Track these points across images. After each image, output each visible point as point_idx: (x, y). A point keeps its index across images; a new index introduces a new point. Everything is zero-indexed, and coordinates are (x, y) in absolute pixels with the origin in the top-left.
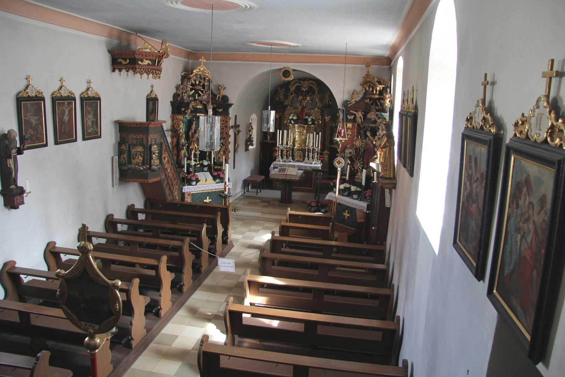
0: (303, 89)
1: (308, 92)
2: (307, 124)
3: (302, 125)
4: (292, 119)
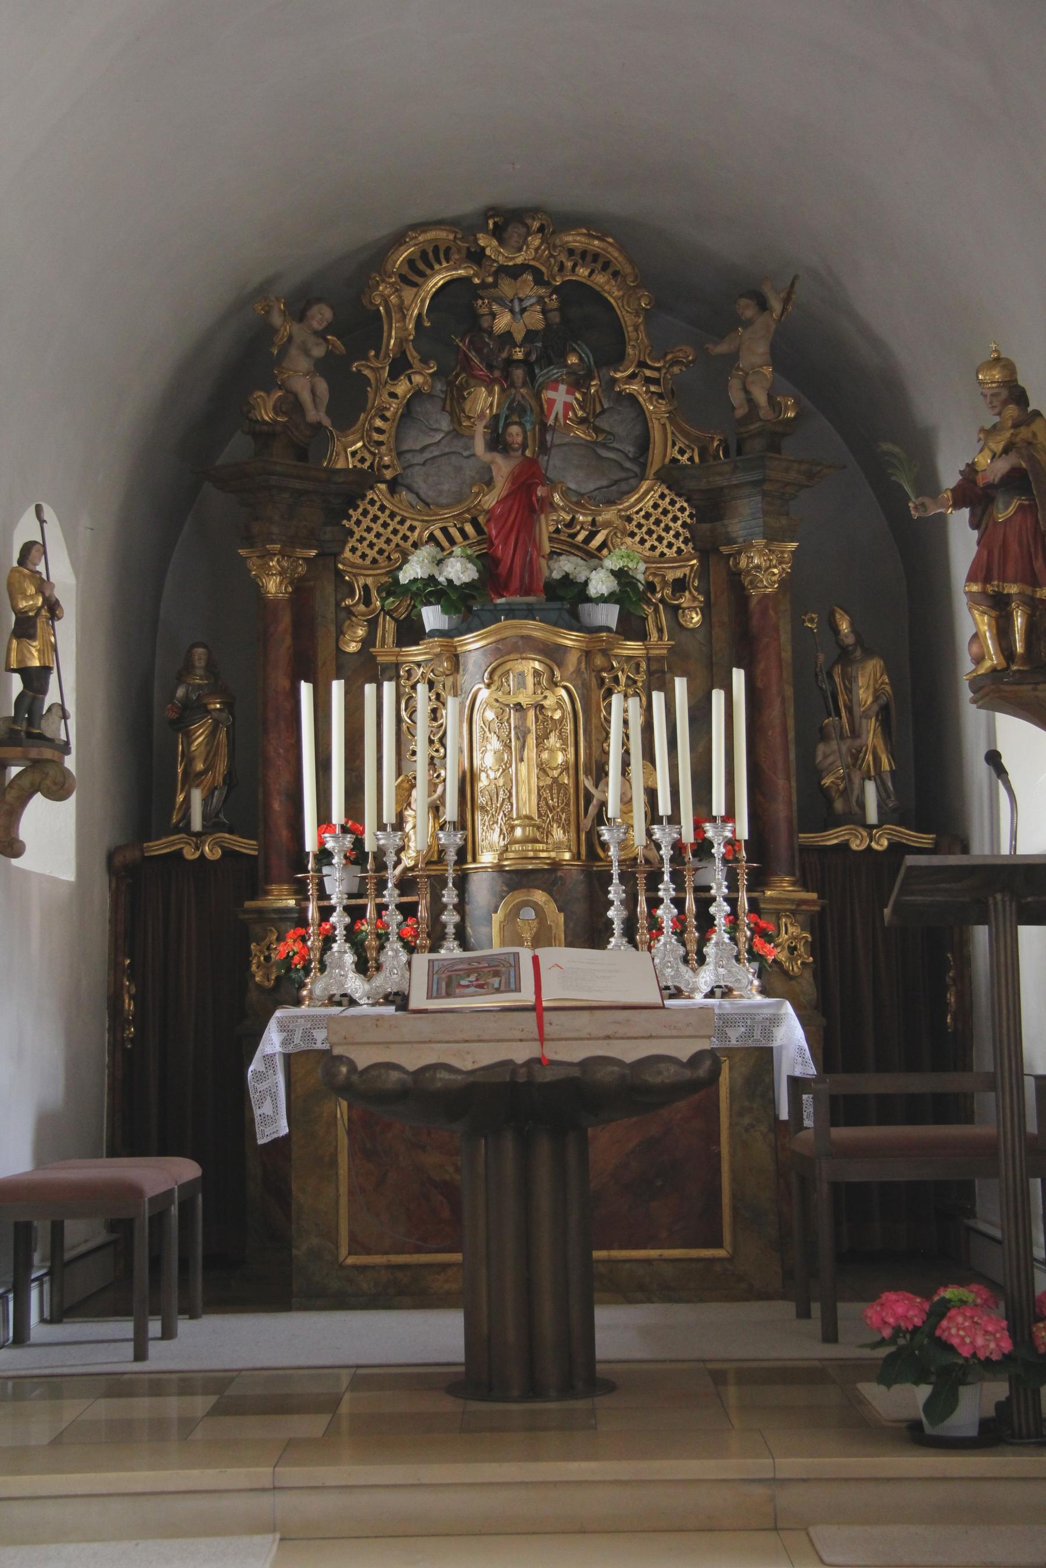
1: (549, 346)
2: (574, 622)
3: (534, 628)
4: (432, 590)
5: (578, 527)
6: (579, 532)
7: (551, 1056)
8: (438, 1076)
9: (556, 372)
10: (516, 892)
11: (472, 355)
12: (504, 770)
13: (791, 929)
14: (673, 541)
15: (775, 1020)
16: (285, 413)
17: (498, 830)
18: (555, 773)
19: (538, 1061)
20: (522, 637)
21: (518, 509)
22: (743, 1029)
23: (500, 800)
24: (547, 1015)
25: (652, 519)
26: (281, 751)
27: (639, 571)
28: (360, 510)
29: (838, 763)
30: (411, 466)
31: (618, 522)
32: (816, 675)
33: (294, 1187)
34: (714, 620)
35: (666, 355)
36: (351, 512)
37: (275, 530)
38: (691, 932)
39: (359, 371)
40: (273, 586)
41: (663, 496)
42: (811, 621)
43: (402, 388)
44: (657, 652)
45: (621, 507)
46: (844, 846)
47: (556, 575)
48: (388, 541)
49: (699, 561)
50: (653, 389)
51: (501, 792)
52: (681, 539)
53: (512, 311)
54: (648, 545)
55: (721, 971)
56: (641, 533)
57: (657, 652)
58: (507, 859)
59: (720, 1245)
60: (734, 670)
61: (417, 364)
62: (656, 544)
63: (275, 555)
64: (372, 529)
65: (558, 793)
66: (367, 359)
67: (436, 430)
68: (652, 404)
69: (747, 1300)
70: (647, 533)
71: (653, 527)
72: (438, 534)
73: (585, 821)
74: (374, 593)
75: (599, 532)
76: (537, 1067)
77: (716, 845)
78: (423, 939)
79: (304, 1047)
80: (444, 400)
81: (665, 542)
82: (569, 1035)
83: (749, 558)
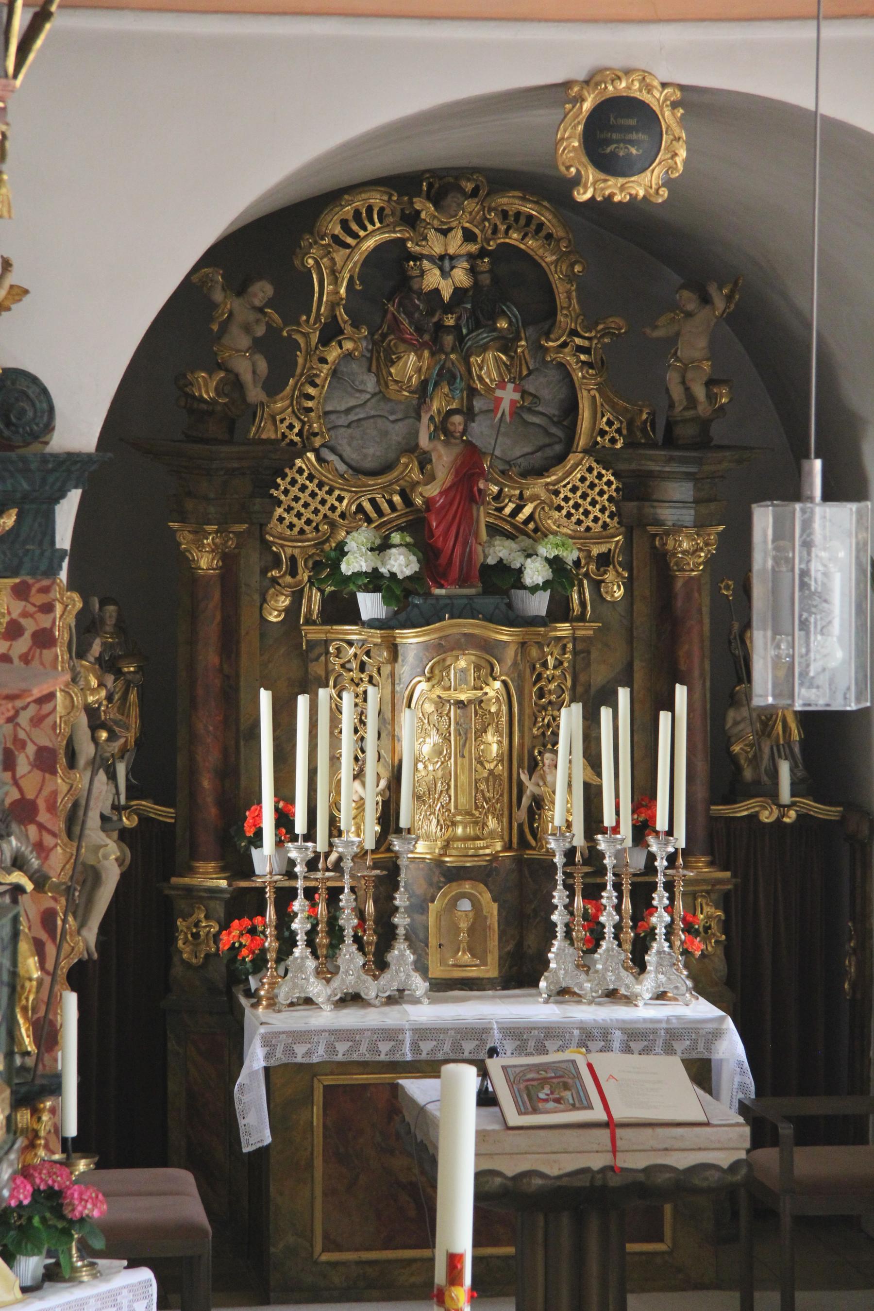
0: (433, 279)
1: (478, 306)
2: (512, 618)
4: (374, 581)
5: (507, 501)
6: (507, 505)
7: (620, 1164)
8: (533, 1181)
9: (484, 336)
10: (454, 884)
11: (402, 317)
12: (442, 763)
13: (707, 909)
14: (599, 515)
15: (717, 1034)
16: (226, 395)
17: (435, 822)
18: (492, 766)
19: (612, 1168)
20: (465, 634)
21: (461, 498)
22: (688, 1043)
23: (438, 791)
24: (619, 1132)
25: (579, 493)
26: (211, 728)
27: (570, 556)
28: (288, 479)
29: (749, 729)
30: (335, 427)
31: (544, 495)
32: (730, 642)
33: (272, 1189)
34: (636, 593)
35: (597, 324)
36: (279, 480)
37: (212, 509)
38: (627, 932)
39: (290, 335)
40: (205, 562)
41: (590, 470)
42: (727, 588)
43: (333, 354)
44: (583, 632)
45: (548, 480)
46: (753, 818)
47: (491, 561)
48: (316, 512)
49: (625, 538)
50: (583, 357)
51: (439, 784)
52: (607, 513)
53: (441, 269)
54: (574, 519)
55: (661, 976)
56: (567, 507)
57: (583, 632)
58: (450, 856)
59: (661, 1240)
60: (678, 686)
61: (348, 330)
62: (582, 518)
63: (210, 534)
64: (299, 498)
65: (494, 784)
66: (299, 324)
67: (361, 391)
68: (582, 371)
69: (684, 1290)
70: (573, 507)
71: (580, 501)
72: (367, 506)
73: (519, 813)
74: (301, 563)
75: (524, 506)
76: (610, 1174)
77: (659, 859)
78: (369, 935)
79: (285, 1060)
80: (370, 360)
81: (591, 517)
82: (635, 1147)
83: (676, 540)
